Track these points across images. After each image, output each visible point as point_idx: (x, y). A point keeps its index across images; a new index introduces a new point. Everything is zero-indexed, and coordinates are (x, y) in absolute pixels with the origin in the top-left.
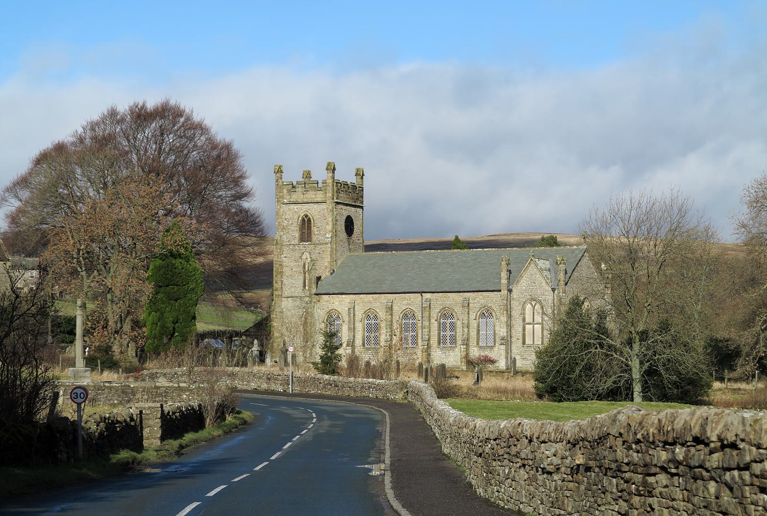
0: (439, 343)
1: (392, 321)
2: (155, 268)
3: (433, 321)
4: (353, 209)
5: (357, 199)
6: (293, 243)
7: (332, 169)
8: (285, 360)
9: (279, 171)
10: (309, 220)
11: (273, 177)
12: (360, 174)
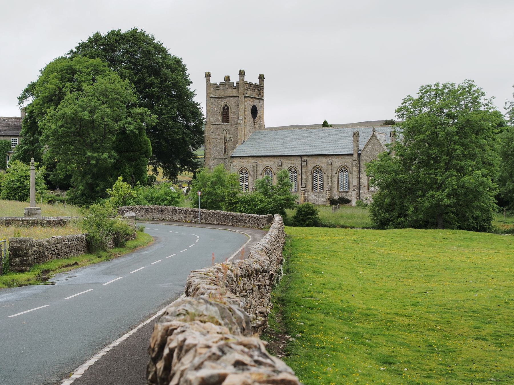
4: (257, 101)
6: (217, 123)
7: (242, 74)
9: (208, 76)
10: (228, 108)
12: (261, 78)
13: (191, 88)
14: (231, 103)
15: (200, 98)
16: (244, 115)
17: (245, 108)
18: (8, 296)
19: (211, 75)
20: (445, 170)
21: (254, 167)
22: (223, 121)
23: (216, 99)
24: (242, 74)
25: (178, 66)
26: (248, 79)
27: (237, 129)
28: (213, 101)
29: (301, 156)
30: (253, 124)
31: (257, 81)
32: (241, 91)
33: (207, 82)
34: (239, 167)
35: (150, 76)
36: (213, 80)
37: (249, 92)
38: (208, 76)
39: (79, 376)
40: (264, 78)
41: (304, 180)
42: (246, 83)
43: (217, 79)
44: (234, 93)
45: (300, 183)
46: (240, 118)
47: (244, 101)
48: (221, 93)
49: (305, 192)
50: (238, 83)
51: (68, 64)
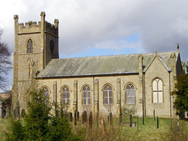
6: (23, 53)
7: (43, 15)
9: (16, 18)
10: (32, 41)
11: (13, 21)
19: (19, 17)
21: (54, 85)
22: (28, 52)
23: (23, 36)
28: (20, 36)
33: (15, 23)
36: (20, 21)
38: (16, 18)
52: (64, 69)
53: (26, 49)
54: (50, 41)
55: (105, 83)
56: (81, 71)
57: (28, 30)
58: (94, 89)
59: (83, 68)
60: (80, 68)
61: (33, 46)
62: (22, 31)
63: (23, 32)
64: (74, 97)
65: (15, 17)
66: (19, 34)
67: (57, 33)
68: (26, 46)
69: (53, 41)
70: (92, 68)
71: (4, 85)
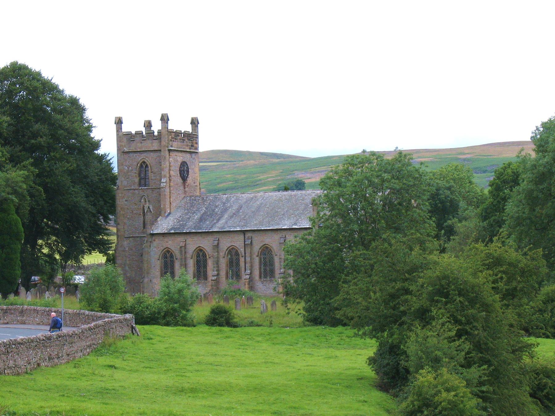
0: (260, 277)
1: (218, 258)
2: (497, 259)
3: (255, 256)
4: (188, 155)
5: (192, 146)
6: (133, 188)
7: (165, 119)
8: (215, 343)
9: (119, 122)
10: (147, 166)
11: (114, 127)
12: (195, 122)
13: (95, 135)
14: (150, 159)
15: (109, 148)
16: (168, 175)
17: (170, 166)
18: (7, 316)
19: (124, 121)
20: (384, 246)
21: (181, 247)
22: (140, 185)
23: (131, 155)
24: (165, 119)
25: (74, 107)
26: (173, 126)
27: (160, 195)
28: (126, 156)
29: (244, 232)
30: (182, 188)
31: (188, 128)
32: (163, 143)
33: (117, 131)
34: (162, 248)
35: (36, 122)
36: (125, 128)
37: (175, 144)
38: (119, 122)
39: (20, 408)
40: (198, 123)
41: (248, 265)
42: (171, 132)
43: (133, 126)
44: (155, 146)
45: (243, 269)
46: (163, 180)
47: (168, 156)
48: (137, 146)
49: (251, 280)
50: (159, 132)
51: (216, 305)
52: (201, 218)
53: (137, 180)
54: (180, 164)
55: (262, 245)
56: (226, 223)
57: (139, 145)
58: (245, 254)
59: (231, 217)
60: (226, 216)
61: (150, 174)
62: (130, 147)
63: (133, 149)
64: (214, 267)
65: (117, 122)
66: (124, 153)
67: (195, 145)
68: (137, 175)
69: (186, 163)
70: (245, 216)
71: (122, 348)
